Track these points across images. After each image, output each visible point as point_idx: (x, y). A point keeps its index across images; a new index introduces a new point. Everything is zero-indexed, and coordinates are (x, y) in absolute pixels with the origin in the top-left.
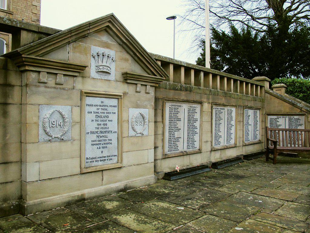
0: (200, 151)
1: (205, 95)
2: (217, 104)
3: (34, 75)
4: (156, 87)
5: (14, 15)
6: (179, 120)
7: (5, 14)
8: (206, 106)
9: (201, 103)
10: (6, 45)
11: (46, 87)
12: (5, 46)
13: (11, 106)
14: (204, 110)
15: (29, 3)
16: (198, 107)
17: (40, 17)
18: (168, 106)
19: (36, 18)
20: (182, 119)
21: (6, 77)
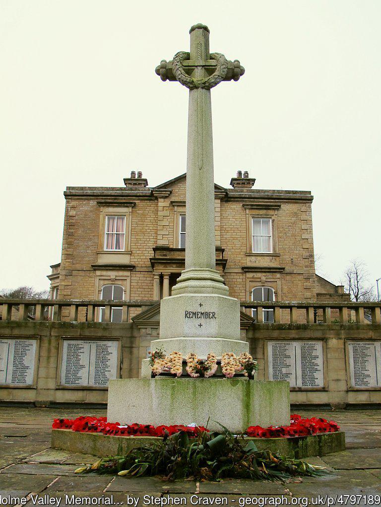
0: (324, 390)
1: (332, 331)
2: (354, 339)
3: (144, 330)
4: (246, 329)
5: (281, 257)
6: (289, 357)
7: (271, 257)
8: (333, 342)
9: (324, 339)
10: (275, 293)
11: (151, 336)
12: (274, 295)
13: (134, 348)
14: (329, 347)
15: (298, 238)
16: (319, 346)
17: (313, 251)
18: (270, 347)
19: (308, 254)
20: (293, 357)
21: (132, 333)
